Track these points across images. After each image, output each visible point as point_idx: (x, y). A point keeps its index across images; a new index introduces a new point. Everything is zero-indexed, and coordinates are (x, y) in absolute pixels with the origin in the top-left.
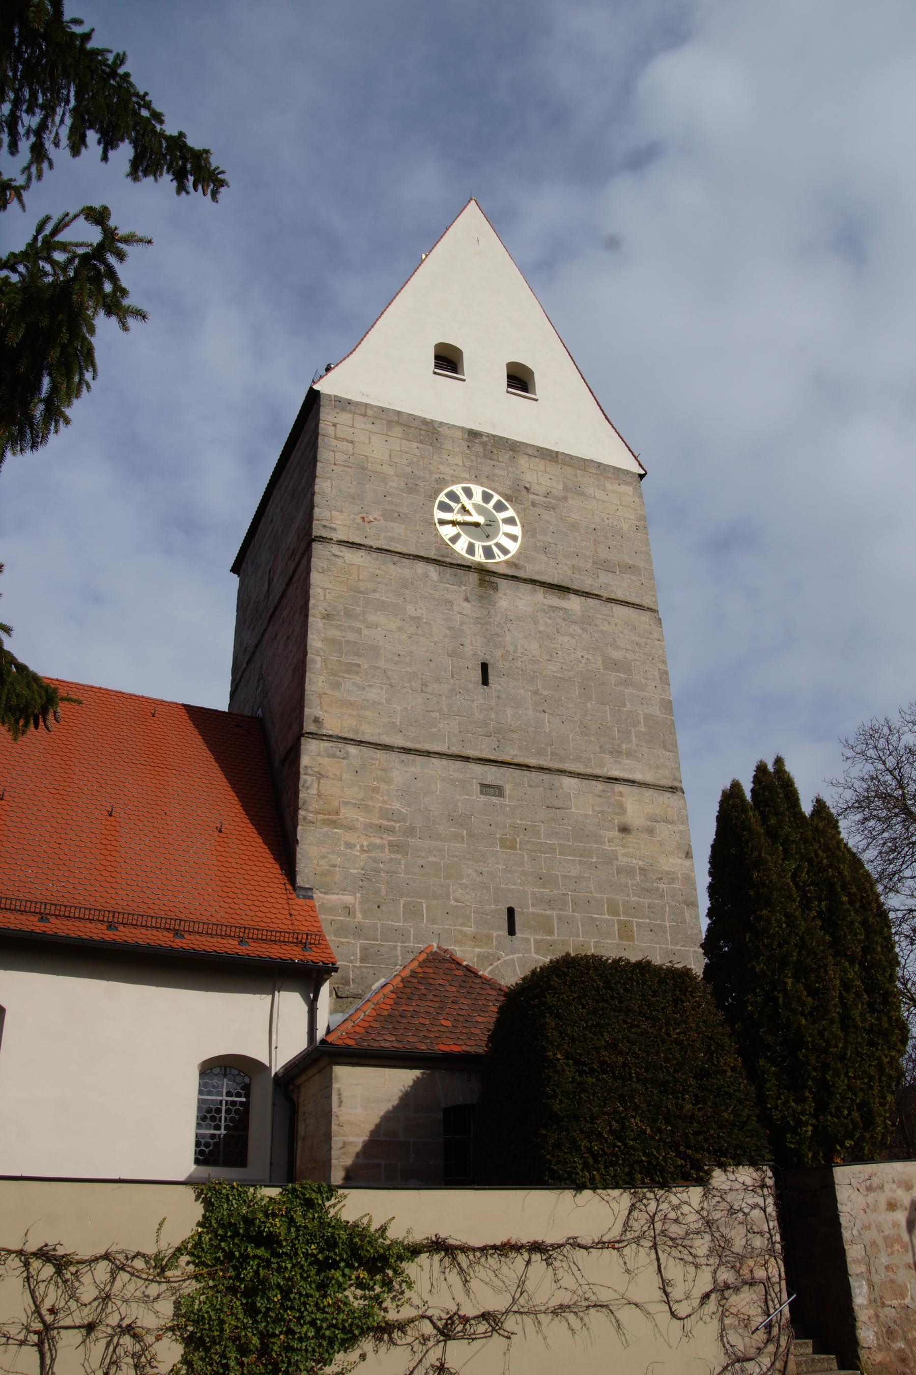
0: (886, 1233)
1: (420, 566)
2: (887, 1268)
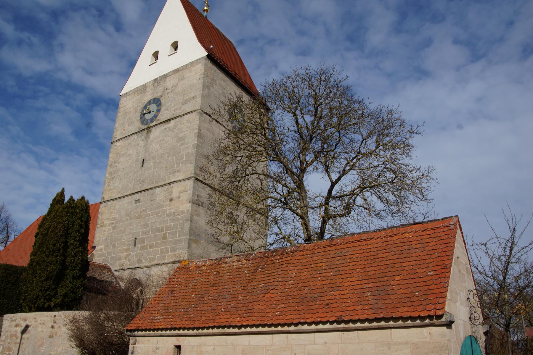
1: (133, 136)
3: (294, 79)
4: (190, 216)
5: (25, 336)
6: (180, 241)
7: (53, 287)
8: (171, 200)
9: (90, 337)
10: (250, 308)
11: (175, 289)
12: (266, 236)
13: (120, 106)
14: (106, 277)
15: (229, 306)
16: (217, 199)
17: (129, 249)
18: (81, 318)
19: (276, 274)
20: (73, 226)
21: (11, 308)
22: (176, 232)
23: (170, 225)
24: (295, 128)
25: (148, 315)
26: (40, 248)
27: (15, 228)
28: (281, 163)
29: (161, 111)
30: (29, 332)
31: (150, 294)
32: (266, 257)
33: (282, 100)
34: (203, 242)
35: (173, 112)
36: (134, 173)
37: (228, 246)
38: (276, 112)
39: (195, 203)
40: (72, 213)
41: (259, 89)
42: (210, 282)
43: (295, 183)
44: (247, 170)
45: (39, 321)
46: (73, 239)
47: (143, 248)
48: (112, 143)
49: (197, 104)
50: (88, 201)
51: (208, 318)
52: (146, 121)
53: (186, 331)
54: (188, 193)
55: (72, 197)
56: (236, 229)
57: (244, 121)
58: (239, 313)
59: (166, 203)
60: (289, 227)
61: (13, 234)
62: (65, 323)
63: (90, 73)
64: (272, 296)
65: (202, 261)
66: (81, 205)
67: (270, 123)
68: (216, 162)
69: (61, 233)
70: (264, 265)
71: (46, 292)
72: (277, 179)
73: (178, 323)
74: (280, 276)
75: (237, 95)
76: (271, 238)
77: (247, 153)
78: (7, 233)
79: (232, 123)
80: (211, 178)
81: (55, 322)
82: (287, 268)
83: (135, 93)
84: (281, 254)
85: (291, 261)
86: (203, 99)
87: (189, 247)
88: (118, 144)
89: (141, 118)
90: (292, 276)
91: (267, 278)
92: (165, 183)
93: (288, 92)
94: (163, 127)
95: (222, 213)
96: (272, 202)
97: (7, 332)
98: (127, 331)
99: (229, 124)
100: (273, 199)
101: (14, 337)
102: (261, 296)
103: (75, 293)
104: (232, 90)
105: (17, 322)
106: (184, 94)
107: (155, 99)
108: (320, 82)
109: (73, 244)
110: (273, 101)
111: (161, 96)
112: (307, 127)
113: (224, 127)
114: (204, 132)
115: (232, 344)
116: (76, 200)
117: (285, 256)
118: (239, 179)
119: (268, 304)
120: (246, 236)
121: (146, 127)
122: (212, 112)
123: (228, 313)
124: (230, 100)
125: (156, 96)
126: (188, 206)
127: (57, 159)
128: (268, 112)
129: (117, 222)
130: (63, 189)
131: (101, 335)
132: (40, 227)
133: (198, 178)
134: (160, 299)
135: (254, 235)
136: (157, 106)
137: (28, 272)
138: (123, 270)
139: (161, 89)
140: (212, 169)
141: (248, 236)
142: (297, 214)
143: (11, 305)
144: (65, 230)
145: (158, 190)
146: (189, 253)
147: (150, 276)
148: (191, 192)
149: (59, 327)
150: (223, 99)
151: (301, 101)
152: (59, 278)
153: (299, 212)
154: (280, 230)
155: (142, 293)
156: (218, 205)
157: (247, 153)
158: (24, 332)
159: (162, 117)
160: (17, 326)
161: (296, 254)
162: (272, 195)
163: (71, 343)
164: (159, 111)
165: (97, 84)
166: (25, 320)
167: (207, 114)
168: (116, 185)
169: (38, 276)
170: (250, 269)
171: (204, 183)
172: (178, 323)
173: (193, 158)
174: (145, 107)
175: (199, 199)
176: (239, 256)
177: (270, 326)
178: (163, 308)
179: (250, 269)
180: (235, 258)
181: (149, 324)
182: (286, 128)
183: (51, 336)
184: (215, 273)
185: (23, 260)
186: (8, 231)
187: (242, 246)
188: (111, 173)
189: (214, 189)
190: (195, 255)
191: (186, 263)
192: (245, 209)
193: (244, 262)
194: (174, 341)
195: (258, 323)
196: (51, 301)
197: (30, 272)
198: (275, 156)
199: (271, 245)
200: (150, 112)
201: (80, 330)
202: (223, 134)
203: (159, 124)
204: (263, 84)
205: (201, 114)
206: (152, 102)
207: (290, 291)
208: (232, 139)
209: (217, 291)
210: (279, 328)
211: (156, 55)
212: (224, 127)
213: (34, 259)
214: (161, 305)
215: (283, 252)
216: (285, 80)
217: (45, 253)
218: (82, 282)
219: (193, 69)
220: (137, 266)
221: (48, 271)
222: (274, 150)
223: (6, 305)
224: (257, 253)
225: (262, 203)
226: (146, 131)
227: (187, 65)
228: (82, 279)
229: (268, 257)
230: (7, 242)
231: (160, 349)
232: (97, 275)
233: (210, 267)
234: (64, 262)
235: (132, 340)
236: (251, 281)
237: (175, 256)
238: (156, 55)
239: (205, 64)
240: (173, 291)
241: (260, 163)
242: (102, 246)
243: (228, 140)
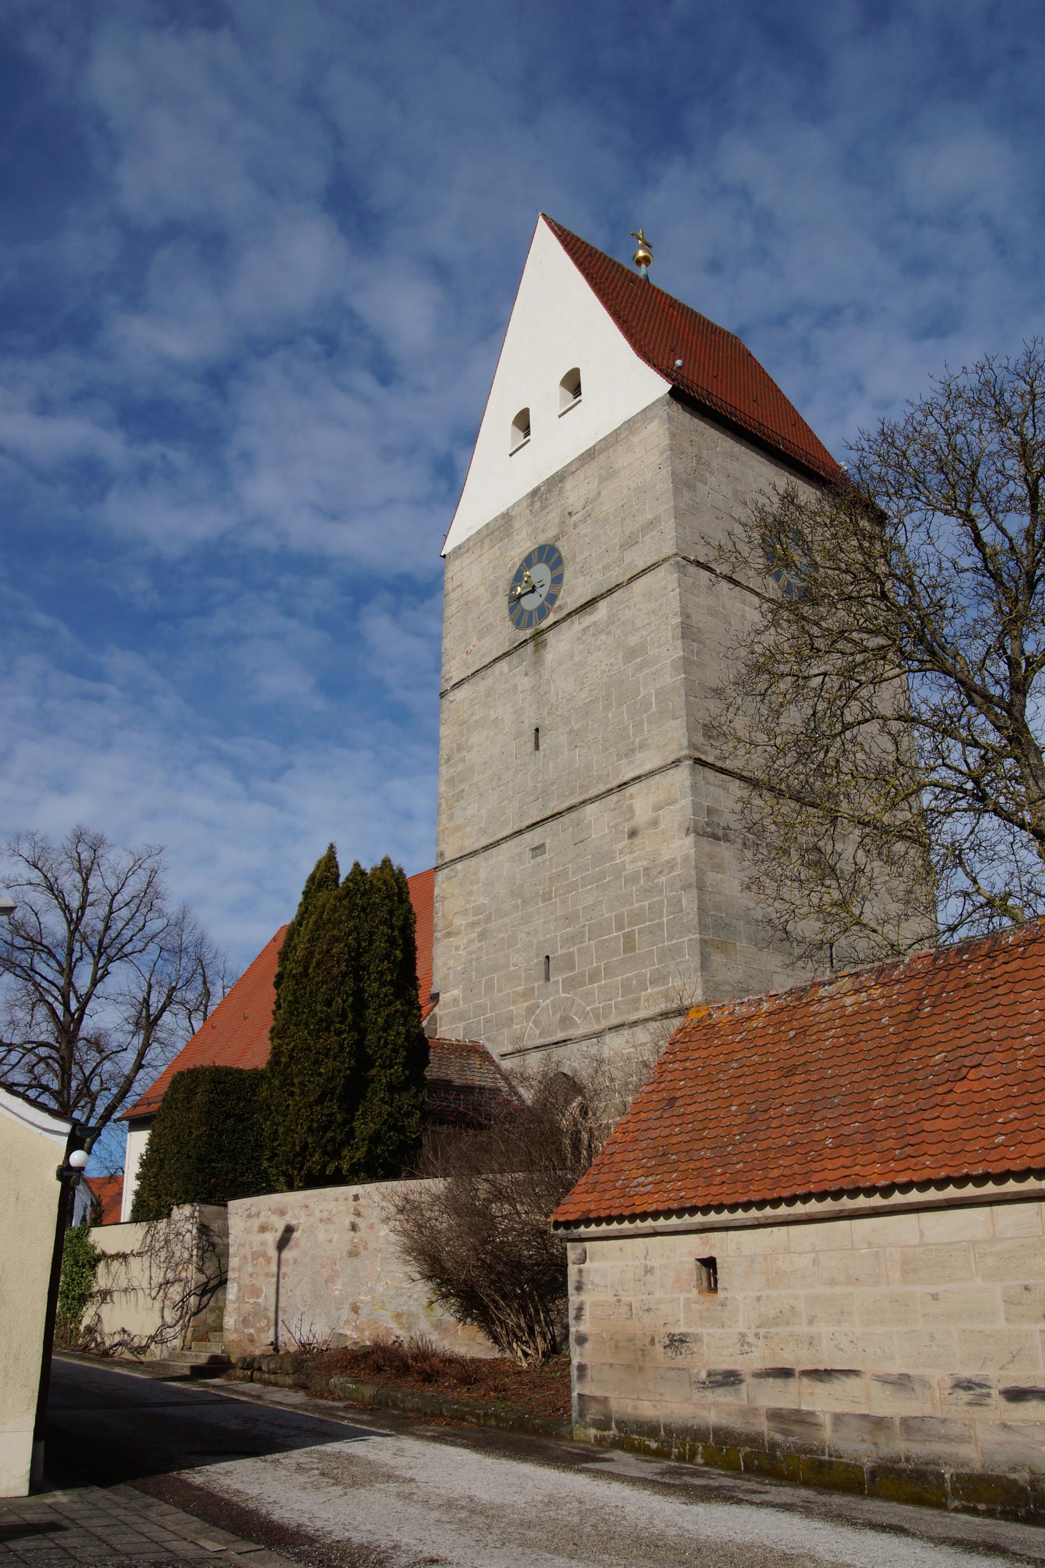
0: (255, 1249)
2: (251, 1276)
3: (948, 408)
4: (693, 872)
5: (286, 1254)
6: (674, 952)
7: (339, 1117)
8: (633, 834)
9: (457, 1250)
10: (911, 1130)
11: (679, 1094)
12: (932, 906)
13: (449, 586)
14: (478, 1076)
15: (847, 1130)
16: (768, 810)
17: (532, 990)
18: (425, 1198)
19: (979, 1017)
20: (370, 944)
21: (243, 1184)
22: (660, 925)
23: (641, 908)
24: (971, 560)
25: (611, 1176)
26: (291, 1013)
27: (221, 967)
28: (948, 673)
29: (565, 580)
30: (297, 1245)
31: (609, 1116)
32: (941, 969)
33: (920, 481)
34: (743, 944)
35: (599, 576)
36: (517, 772)
37: (820, 948)
38: (907, 520)
39: (705, 834)
40: (364, 909)
41: (845, 461)
42: (780, 1064)
43: (998, 728)
44: (846, 711)
45: (318, 1214)
46: (375, 979)
47: (570, 984)
48: (442, 695)
49: (664, 541)
50: (401, 871)
51: (787, 1172)
52: (525, 618)
53: (726, 1216)
54: (678, 806)
55: (357, 865)
56: (836, 895)
57: (815, 565)
58: (879, 1147)
59: (619, 846)
60: (1001, 869)
61: (220, 983)
62: (384, 1214)
63: (334, 517)
64: (976, 1086)
65: (750, 1004)
66: (385, 883)
67: (894, 557)
68: (750, 705)
69: (343, 968)
70: (939, 995)
71: (325, 1133)
72: (944, 726)
73: (701, 1191)
74: (991, 1024)
75: (781, 491)
76: (950, 910)
77: (836, 661)
78: (205, 983)
79: (777, 577)
80: (741, 752)
81: (358, 1214)
82: (1012, 996)
83: (482, 542)
84: (987, 955)
85: (1021, 974)
86: (680, 524)
87: (704, 966)
88: (459, 695)
89: (511, 610)
90: (1029, 1019)
91: (951, 1034)
92: (609, 786)
93: (934, 452)
94: (577, 625)
95: (786, 852)
96: (936, 798)
97: (242, 1245)
98: (557, 1225)
99: (771, 582)
100: (937, 790)
101: (261, 1260)
102: (940, 1090)
103: (401, 1130)
104: (763, 480)
105: (262, 1219)
106: (623, 519)
107: (541, 549)
108: (1033, 401)
109: (377, 996)
110: (892, 491)
111: (557, 538)
112: (1012, 548)
113: (757, 594)
114: (700, 619)
115: (870, 1245)
116: (368, 871)
117: (1001, 958)
118: (825, 742)
119: (965, 1112)
120: (870, 912)
121: (528, 633)
122: (713, 554)
123: (846, 1152)
124: (761, 510)
125: (542, 539)
126: (683, 846)
127: (289, 766)
128: (883, 528)
129: (488, 919)
130: (332, 847)
131: (485, 1242)
132: (284, 956)
133: (703, 757)
134: (639, 1126)
135: (894, 908)
136: (552, 568)
137: (270, 1083)
138: (521, 1052)
139: (553, 516)
140: (740, 725)
141: (876, 911)
142: (1022, 826)
143: (242, 1175)
144: (353, 959)
145: (590, 809)
146: (705, 982)
147: (601, 1062)
148: (686, 802)
149: (372, 1226)
150: (739, 512)
151: (981, 473)
152: (354, 1091)
153: (1028, 818)
154: (975, 881)
155: (586, 1113)
156: (773, 828)
157: (836, 661)
158: (283, 1243)
159: (571, 597)
160: (263, 1229)
161: (1034, 948)
162: (934, 776)
163: (409, 1268)
164: (557, 580)
165: (361, 542)
167: (698, 564)
168: (470, 811)
169: (297, 1091)
170: (897, 1010)
171: (722, 771)
172: (701, 1191)
173: (678, 701)
174: (518, 578)
175: (716, 819)
176: (857, 975)
177: (980, 1180)
178: (650, 1152)
179: (897, 1010)
180: (847, 984)
181: (617, 1202)
182: (946, 564)
183: (353, 1253)
184: (792, 1033)
185: (254, 1054)
186: (204, 976)
187: (862, 945)
188: (451, 781)
189: (753, 783)
190: (726, 988)
191: (704, 1013)
192: (857, 832)
193: (876, 993)
194: (695, 1246)
195: (943, 1174)
196: (340, 1158)
197: (277, 1082)
198: (926, 658)
199: (952, 929)
201: (427, 1232)
202: (756, 617)
203: (564, 619)
204: (852, 443)
205: (681, 570)
206: (535, 558)
207: (1029, 1065)
208: (785, 625)
209: (804, 1087)
210: (1012, 1186)
211: (523, 422)
212: (757, 594)
213: (281, 1046)
214: (644, 1144)
215: (992, 948)
216: (919, 416)
217: (307, 1026)
218: (415, 1096)
219: (635, 440)
220: (560, 1036)
221: (320, 1074)
222: (920, 639)
223: (230, 1176)
224: (912, 961)
225: (904, 805)
226: (531, 646)
227: (616, 432)
228: (413, 1090)
229: (948, 968)
230: (206, 1007)
231: (658, 1273)
232: (453, 1074)
233: (776, 1018)
235: (572, 1252)
236: (906, 1045)
237: (666, 996)
238: (523, 422)
239: (670, 419)
240: (675, 1099)
241: (884, 685)
242: (456, 992)
243: (772, 630)
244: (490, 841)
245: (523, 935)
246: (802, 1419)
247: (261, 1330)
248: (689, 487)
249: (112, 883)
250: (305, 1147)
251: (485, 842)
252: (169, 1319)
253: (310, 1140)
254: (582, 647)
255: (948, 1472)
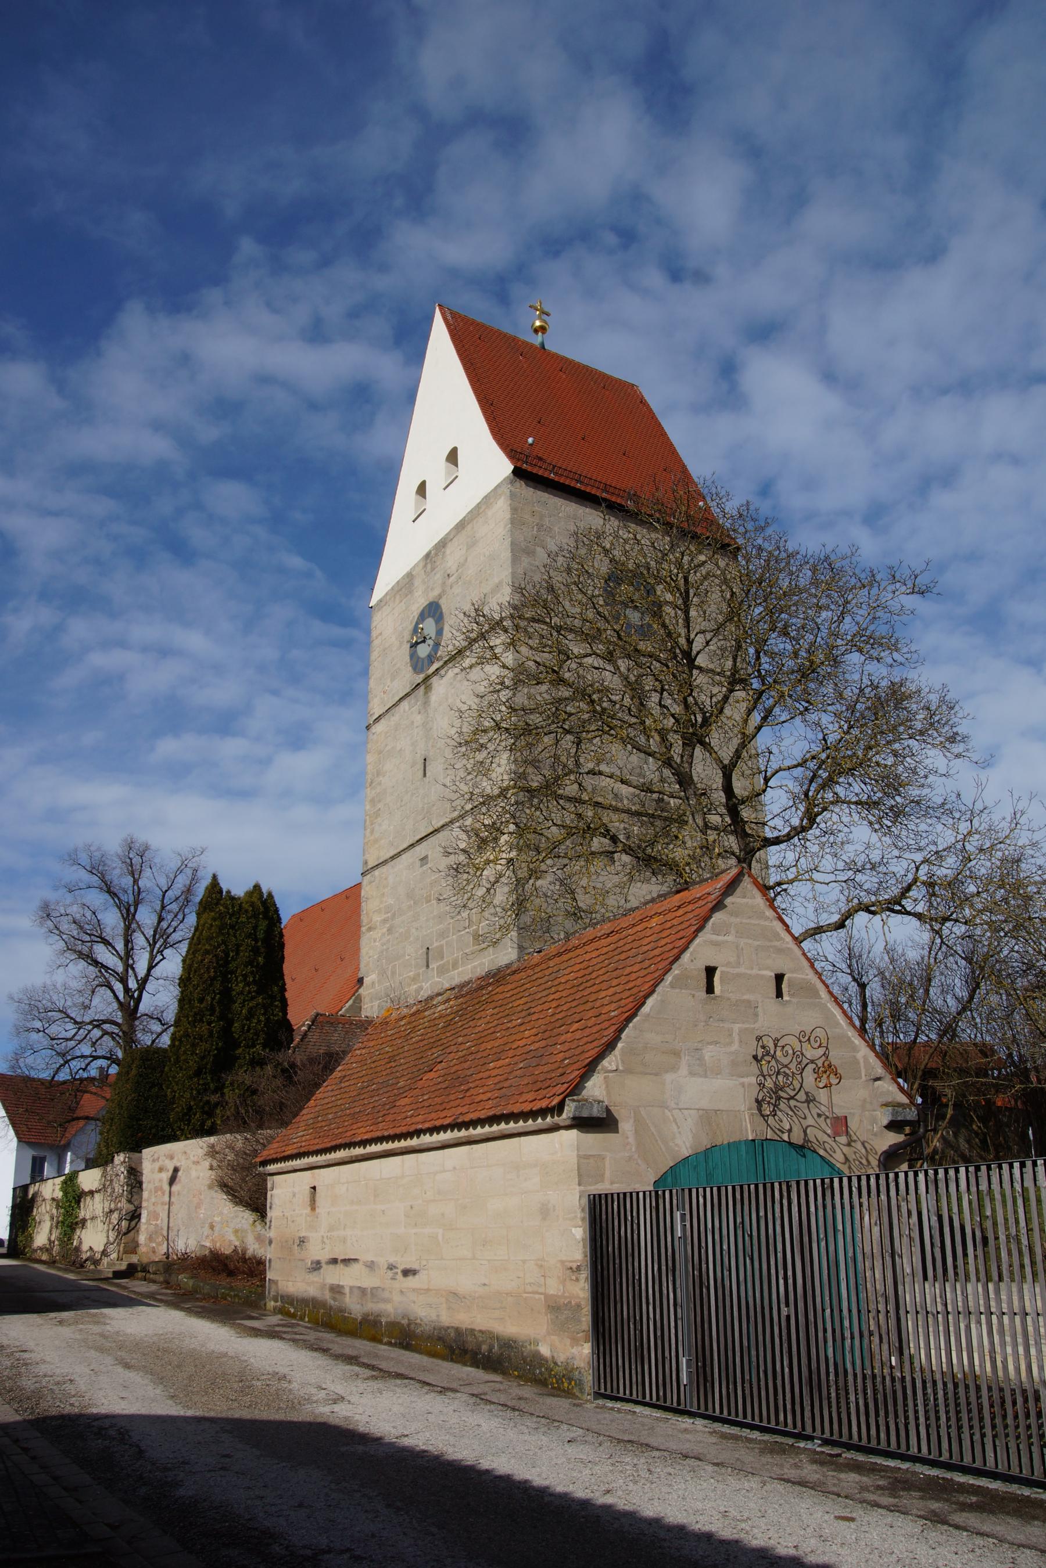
5: (175, 1188)
17: (419, 975)
20: (237, 954)
36: (413, 794)
40: (232, 927)
48: (368, 728)
50: (270, 895)
66: (252, 904)
69: (212, 974)
111: (440, 596)
129: (393, 917)
143: (163, 1129)
158: (172, 1181)
160: (161, 1170)
166: (172, 1158)
194: (306, 1179)
200: (424, 641)
219: (490, 513)
223: (153, 1131)
226: (422, 688)
234: (226, 1031)
238: (422, 490)
244: (395, 852)
245: (414, 930)
246: (336, 1290)
247: (159, 1244)
248: (528, 554)
249: (163, 883)
250: (190, 1108)
251: (392, 854)
252: (111, 1239)
253: (192, 1103)
254: (453, 691)
255: (383, 1320)
